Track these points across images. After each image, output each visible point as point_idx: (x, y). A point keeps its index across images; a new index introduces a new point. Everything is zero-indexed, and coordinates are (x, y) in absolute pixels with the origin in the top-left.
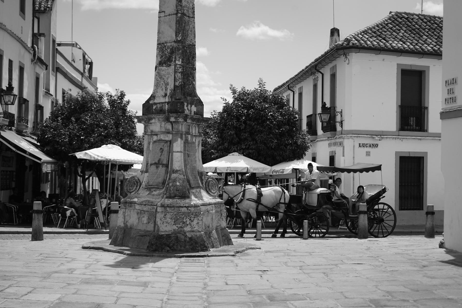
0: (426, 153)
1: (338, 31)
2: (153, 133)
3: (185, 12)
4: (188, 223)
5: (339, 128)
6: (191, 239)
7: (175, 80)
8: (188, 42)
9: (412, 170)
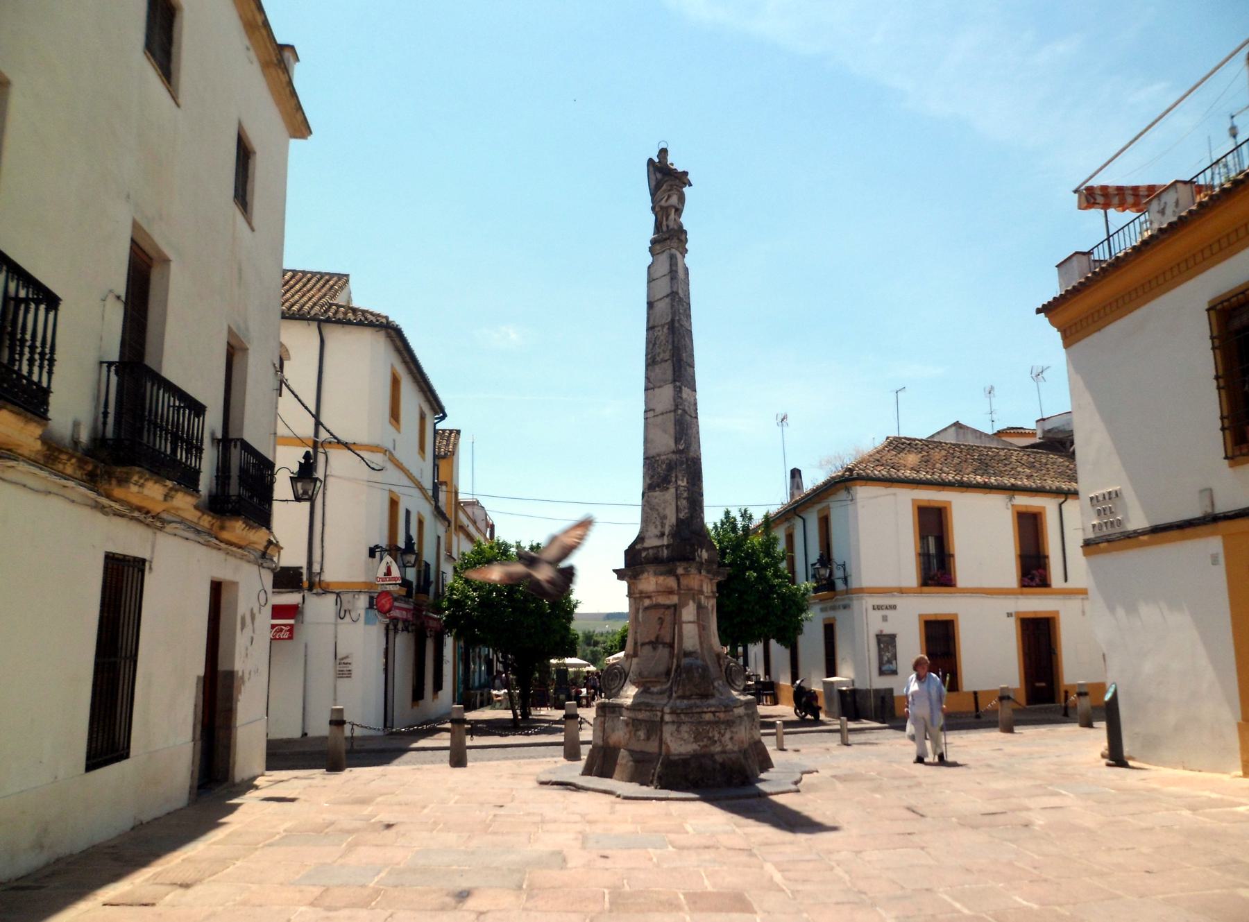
0: (1057, 612)
1: (799, 471)
5: (840, 585)
6: (723, 765)
8: (692, 454)
9: (1039, 638)
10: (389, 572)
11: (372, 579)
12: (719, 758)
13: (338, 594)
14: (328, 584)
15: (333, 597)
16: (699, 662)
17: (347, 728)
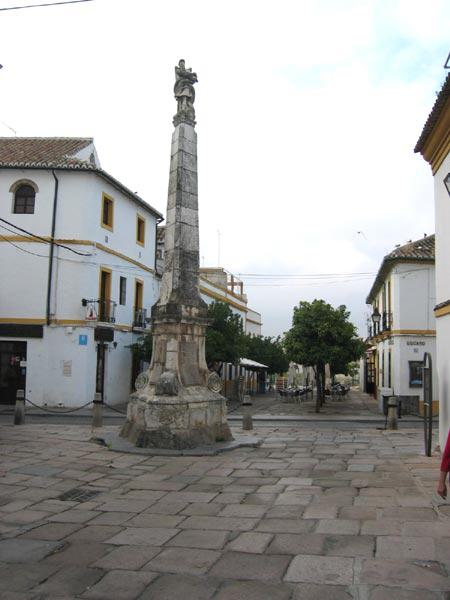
10: (91, 315)
12: (173, 432)
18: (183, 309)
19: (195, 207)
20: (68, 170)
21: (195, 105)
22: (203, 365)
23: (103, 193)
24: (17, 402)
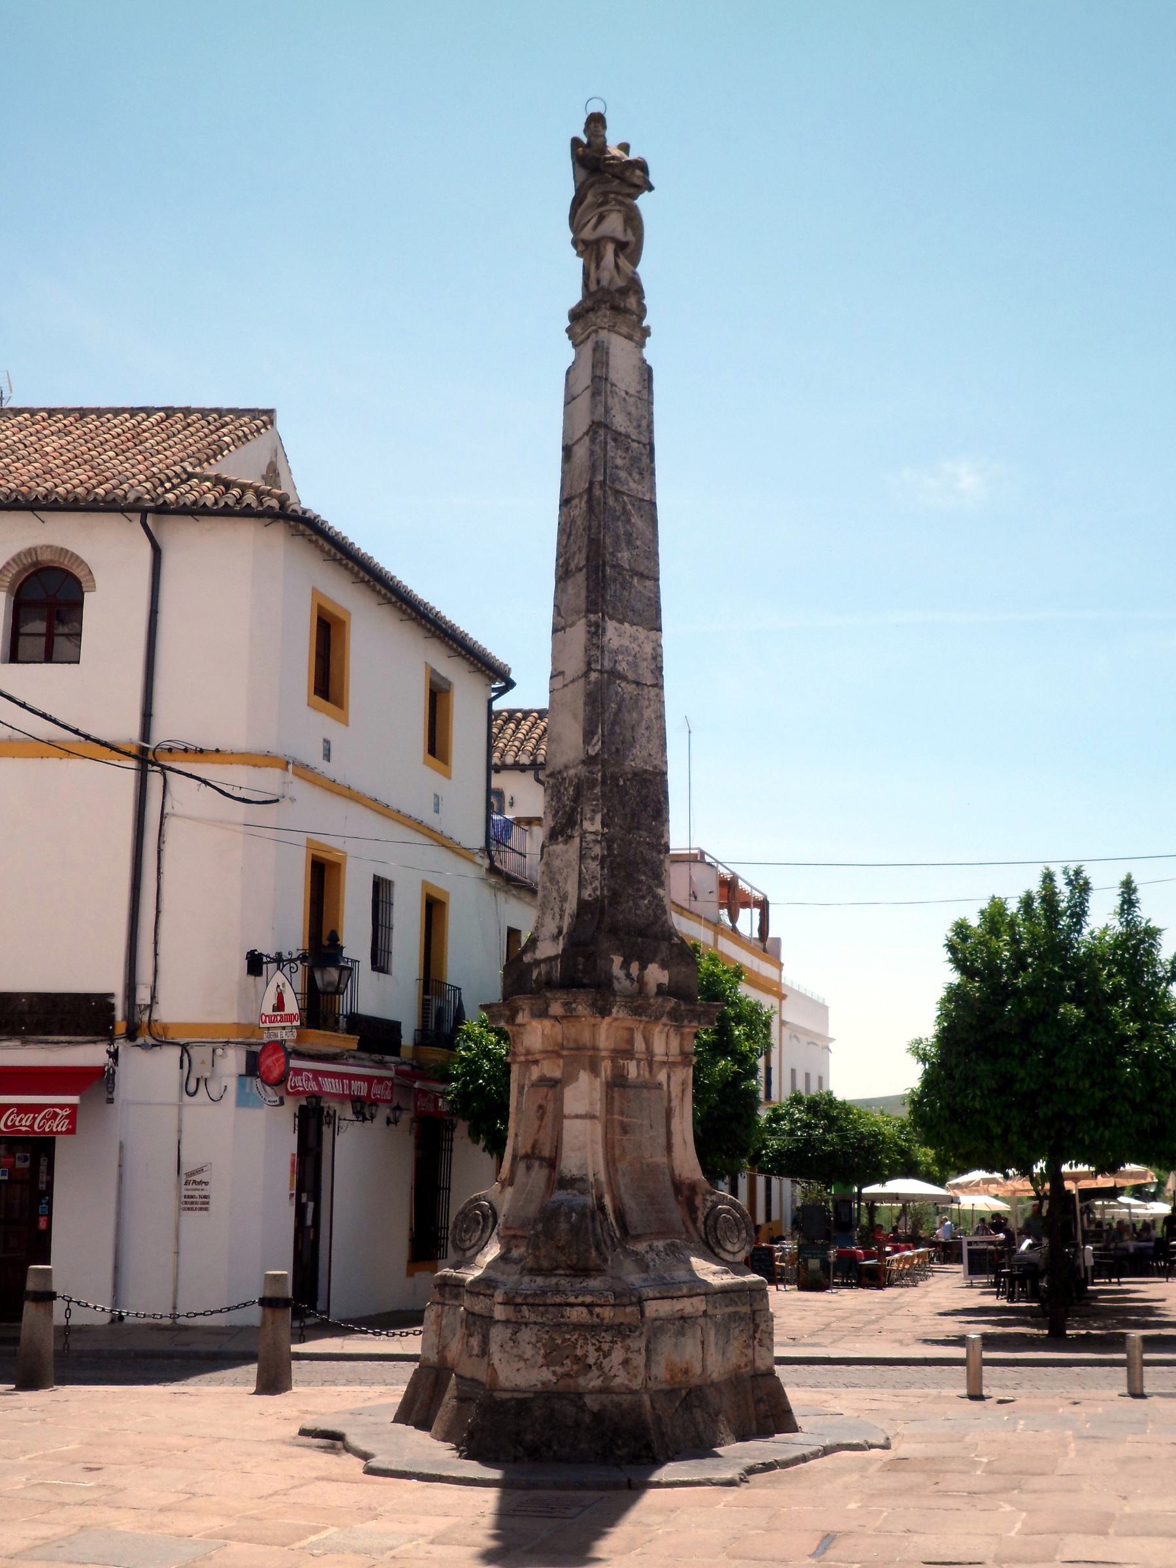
2: (530, 1057)
3: (622, 667)
4: (591, 1361)
6: (598, 1417)
7: (581, 885)
10: (280, 1005)
11: (254, 1019)
12: (591, 1402)
13: (184, 1048)
14: (165, 1027)
15: (176, 1052)
16: (590, 1201)
17: (58, 1306)
18: (617, 969)
19: (649, 617)
20: (196, 511)
21: (644, 270)
22: (687, 1163)
23: (314, 590)
24: (29, 1307)
